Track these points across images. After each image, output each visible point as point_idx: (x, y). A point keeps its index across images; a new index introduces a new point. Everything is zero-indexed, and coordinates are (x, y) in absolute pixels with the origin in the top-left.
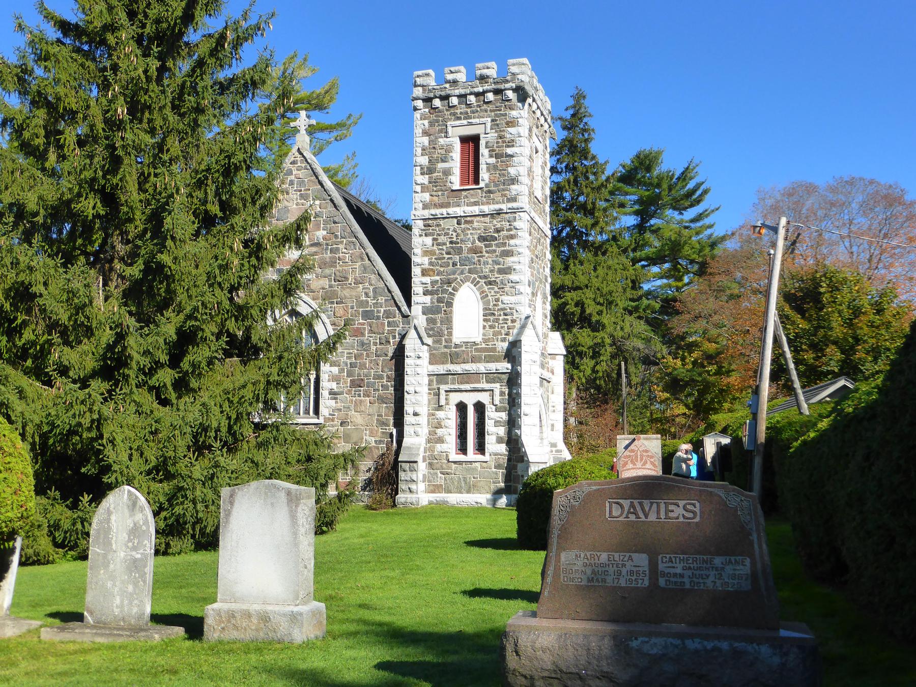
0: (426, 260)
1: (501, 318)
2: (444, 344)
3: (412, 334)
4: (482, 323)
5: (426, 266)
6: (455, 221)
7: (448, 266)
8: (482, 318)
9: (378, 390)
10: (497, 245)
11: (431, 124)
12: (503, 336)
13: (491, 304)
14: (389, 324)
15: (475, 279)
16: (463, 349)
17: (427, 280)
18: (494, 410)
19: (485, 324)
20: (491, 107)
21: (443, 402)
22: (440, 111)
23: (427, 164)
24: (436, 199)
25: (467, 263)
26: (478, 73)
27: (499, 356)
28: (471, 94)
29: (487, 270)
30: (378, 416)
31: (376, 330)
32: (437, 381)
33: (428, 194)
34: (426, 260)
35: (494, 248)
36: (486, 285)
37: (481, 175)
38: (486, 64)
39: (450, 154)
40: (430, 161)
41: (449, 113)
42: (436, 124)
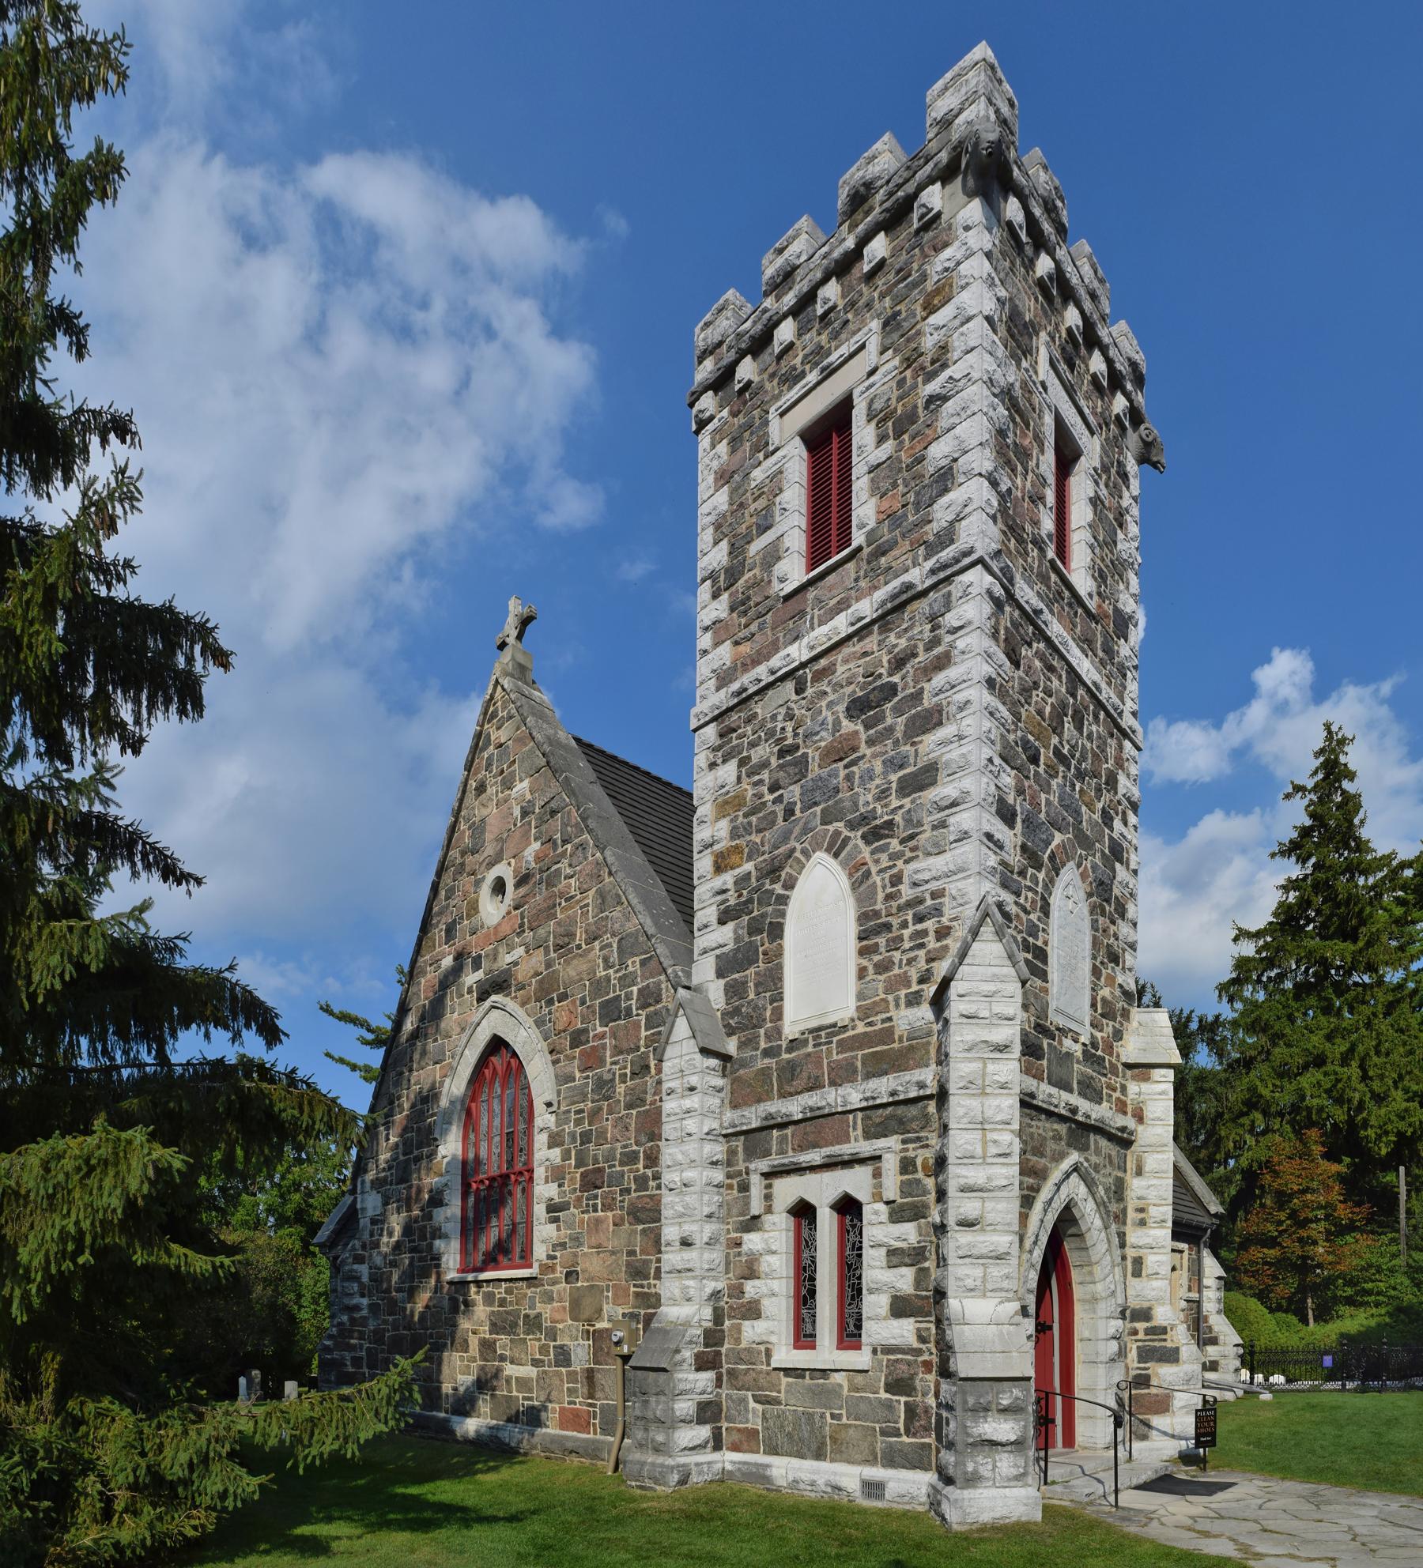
1: (906, 933)
2: (763, 1045)
6: (790, 686)
7: (773, 823)
12: (915, 988)
13: (880, 896)
15: (837, 833)
16: (810, 1049)
17: (728, 879)
18: (884, 1217)
19: (865, 963)
21: (756, 1207)
24: (745, 648)
27: (900, 1050)
29: (870, 798)
32: (746, 1149)
36: (868, 843)
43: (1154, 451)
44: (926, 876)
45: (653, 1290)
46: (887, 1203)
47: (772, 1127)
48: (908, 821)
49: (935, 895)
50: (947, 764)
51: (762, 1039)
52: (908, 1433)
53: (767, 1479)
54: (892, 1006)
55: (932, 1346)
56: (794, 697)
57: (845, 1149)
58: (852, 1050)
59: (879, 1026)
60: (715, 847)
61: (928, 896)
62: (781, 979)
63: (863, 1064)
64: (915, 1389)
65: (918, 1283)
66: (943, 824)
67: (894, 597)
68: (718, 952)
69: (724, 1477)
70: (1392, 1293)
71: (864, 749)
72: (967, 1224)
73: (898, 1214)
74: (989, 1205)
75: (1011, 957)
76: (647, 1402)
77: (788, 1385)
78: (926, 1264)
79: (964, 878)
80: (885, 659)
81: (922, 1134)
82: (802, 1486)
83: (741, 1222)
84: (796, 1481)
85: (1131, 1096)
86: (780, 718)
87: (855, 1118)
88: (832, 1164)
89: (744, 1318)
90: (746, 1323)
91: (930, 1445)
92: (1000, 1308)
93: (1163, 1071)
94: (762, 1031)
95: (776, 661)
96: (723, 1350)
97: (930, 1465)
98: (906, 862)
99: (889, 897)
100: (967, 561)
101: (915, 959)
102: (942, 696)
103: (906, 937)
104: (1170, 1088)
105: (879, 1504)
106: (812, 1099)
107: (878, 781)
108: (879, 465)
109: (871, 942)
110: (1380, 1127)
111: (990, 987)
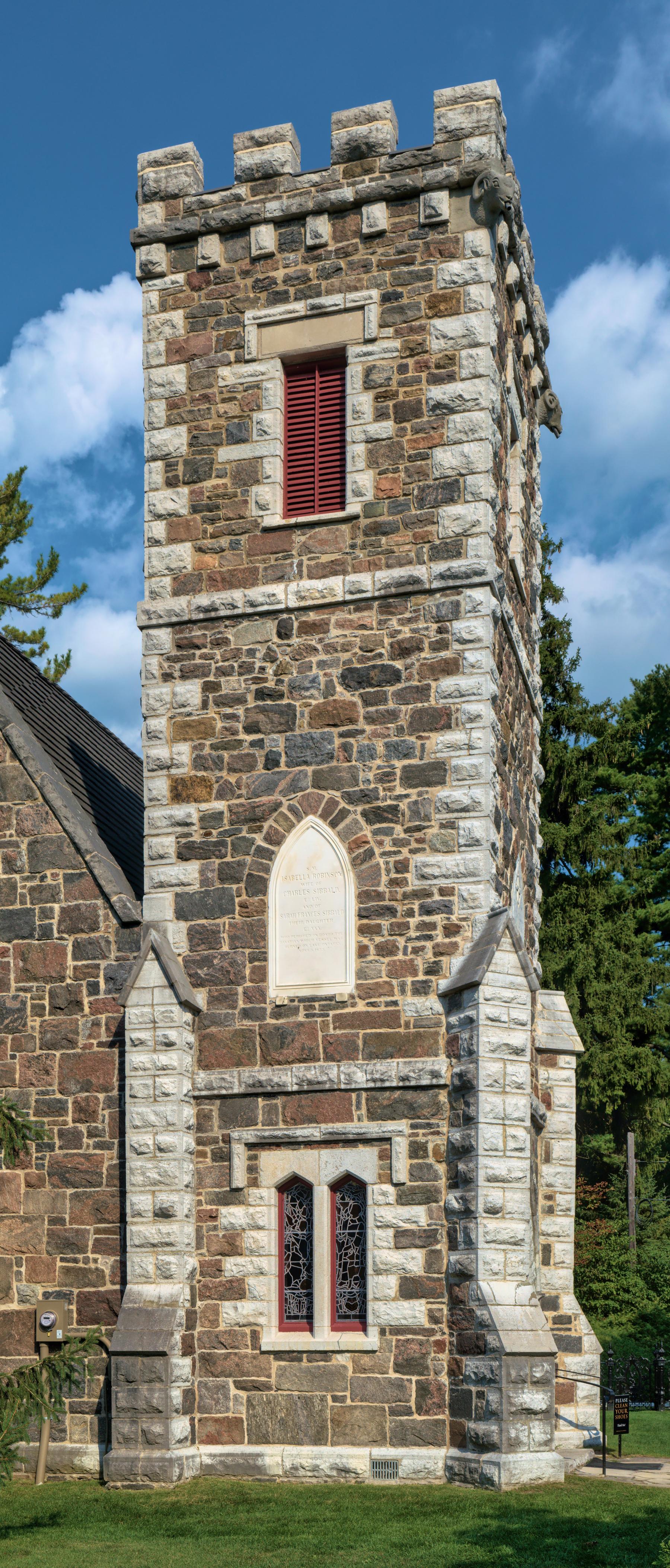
0: (184, 752)
1: (413, 921)
2: (241, 1004)
3: (151, 973)
4: (353, 939)
5: (185, 771)
6: (271, 626)
7: (252, 767)
8: (353, 922)
9: (51, 1147)
10: (402, 697)
11: (195, 322)
12: (421, 977)
13: (384, 879)
14: (79, 951)
15: (333, 803)
16: (301, 1018)
17: (190, 811)
18: (392, 1199)
19: (365, 941)
20: (380, 252)
21: (240, 1178)
22: (223, 280)
23: (184, 449)
24: (211, 560)
25: (308, 755)
26: (340, 137)
27: (407, 1036)
28: (318, 212)
29: (371, 776)
30: (52, 1221)
31: (40, 971)
32: (222, 1115)
33: (188, 545)
34: (184, 752)
35: (391, 705)
36: (369, 822)
37: (349, 479)
38: (366, 108)
39: (256, 416)
40: (194, 442)
41: (249, 281)
42: (212, 321)
43: (554, 416)
44: (436, 872)
45: (92, 1266)
46: (396, 1185)
47: (257, 1095)
48: (415, 813)
49: (442, 891)
50: (457, 769)
51: (241, 997)
52: (419, 1410)
53: (260, 1469)
54: (396, 990)
55: (444, 1326)
56: (276, 639)
57: (351, 1127)
58: (352, 1027)
59: (382, 1009)
60: (173, 771)
61: (435, 891)
62: (264, 938)
63: (365, 1043)
64: (427, 1368)
65: (429, 1265)
66: (451, 825)
67: (399, 584)
68: (178, 889)
69: (207, 1469)
70: (627, 1296)
71: (361, 724)
72: (493, 1211)
73: (406, 1197)
74: (509, 1195)
75: (524, 968)
76: (135, 1390)
77: (280, 1368)
78: (438, 1247)
79: (474, 883)
80: (387, 641)
81: (432, 1121)
82: (301, 1472)
83: (217, 1194)
84: (295, 1468)
85: (541, 1081)
86: (259, 655)
87: (358, 1097)
88: (331, 1142)
89: (222, 1298)
90: (227, 1304)
91: (444, 1421)
92: (519, 1290)
93: (568, 1058)
94: (240, 989)
95: (257, 593)
96: (196, 1333)
97: (444, 1440)
98: (413, 851)
99: (393, 882)
100: (477, 580)
101: (423, 948)
102: (450, 700)
103: (412, 925)
104: (572, 1074)
105: (392, 1482)
106: (312, 1072)
107: (378, 762)
108: (377, 440)
109: (373, 922)
110: (604, 1077)
111: (508, 994)
